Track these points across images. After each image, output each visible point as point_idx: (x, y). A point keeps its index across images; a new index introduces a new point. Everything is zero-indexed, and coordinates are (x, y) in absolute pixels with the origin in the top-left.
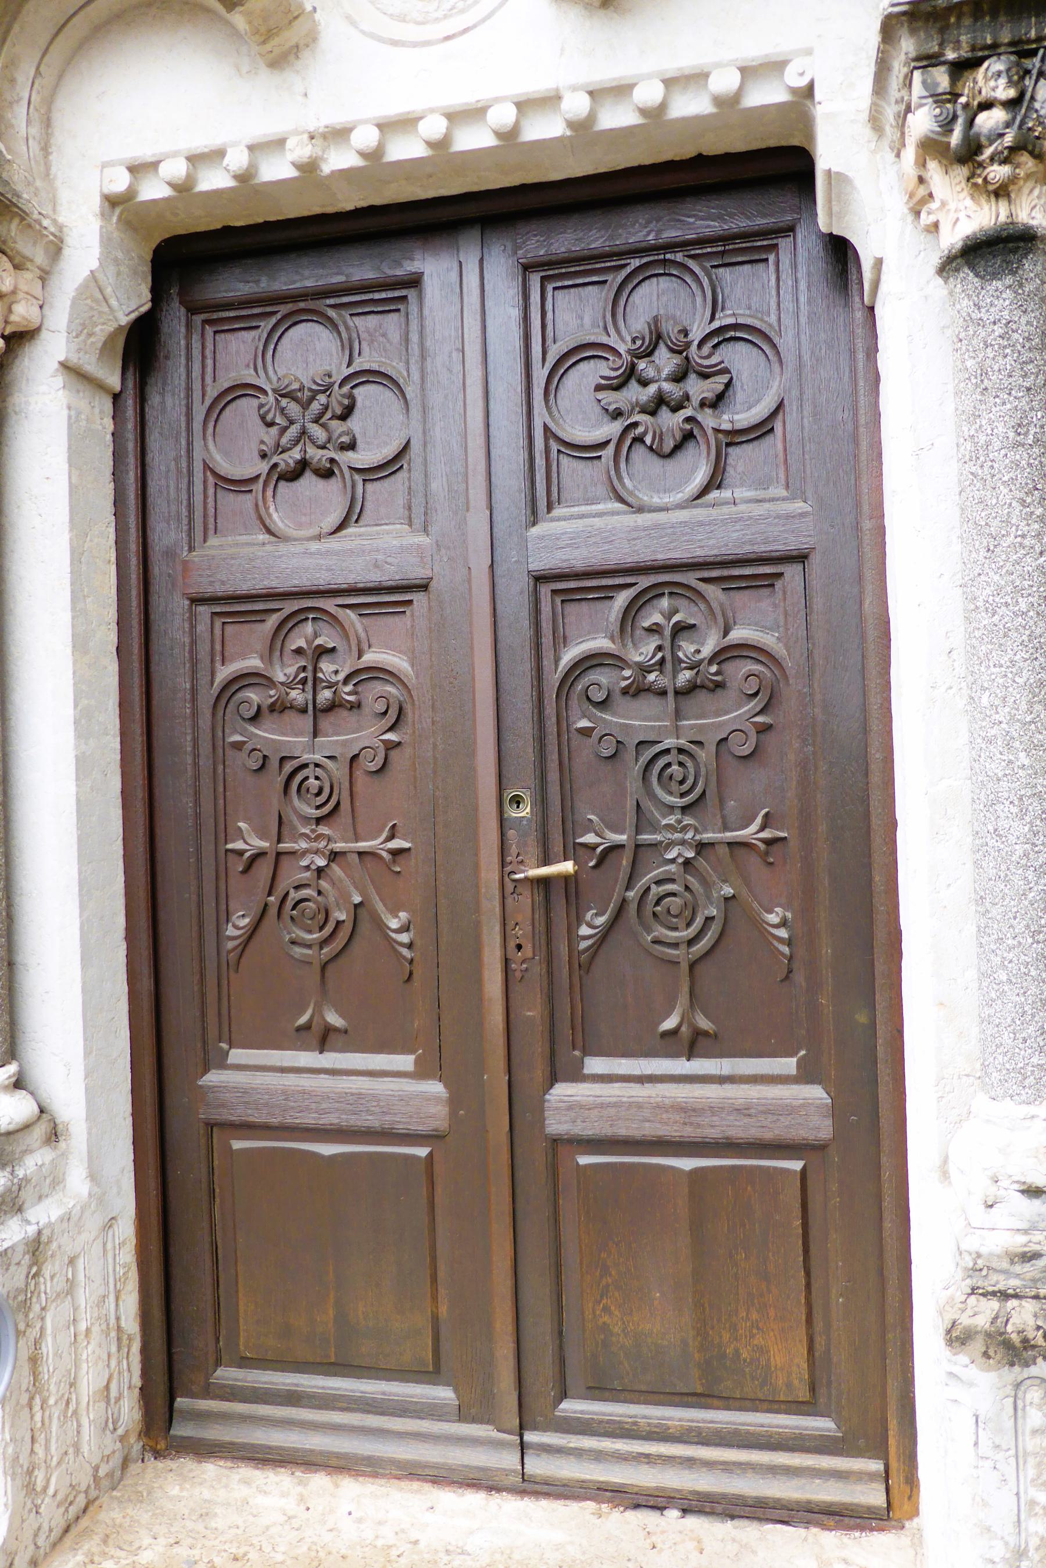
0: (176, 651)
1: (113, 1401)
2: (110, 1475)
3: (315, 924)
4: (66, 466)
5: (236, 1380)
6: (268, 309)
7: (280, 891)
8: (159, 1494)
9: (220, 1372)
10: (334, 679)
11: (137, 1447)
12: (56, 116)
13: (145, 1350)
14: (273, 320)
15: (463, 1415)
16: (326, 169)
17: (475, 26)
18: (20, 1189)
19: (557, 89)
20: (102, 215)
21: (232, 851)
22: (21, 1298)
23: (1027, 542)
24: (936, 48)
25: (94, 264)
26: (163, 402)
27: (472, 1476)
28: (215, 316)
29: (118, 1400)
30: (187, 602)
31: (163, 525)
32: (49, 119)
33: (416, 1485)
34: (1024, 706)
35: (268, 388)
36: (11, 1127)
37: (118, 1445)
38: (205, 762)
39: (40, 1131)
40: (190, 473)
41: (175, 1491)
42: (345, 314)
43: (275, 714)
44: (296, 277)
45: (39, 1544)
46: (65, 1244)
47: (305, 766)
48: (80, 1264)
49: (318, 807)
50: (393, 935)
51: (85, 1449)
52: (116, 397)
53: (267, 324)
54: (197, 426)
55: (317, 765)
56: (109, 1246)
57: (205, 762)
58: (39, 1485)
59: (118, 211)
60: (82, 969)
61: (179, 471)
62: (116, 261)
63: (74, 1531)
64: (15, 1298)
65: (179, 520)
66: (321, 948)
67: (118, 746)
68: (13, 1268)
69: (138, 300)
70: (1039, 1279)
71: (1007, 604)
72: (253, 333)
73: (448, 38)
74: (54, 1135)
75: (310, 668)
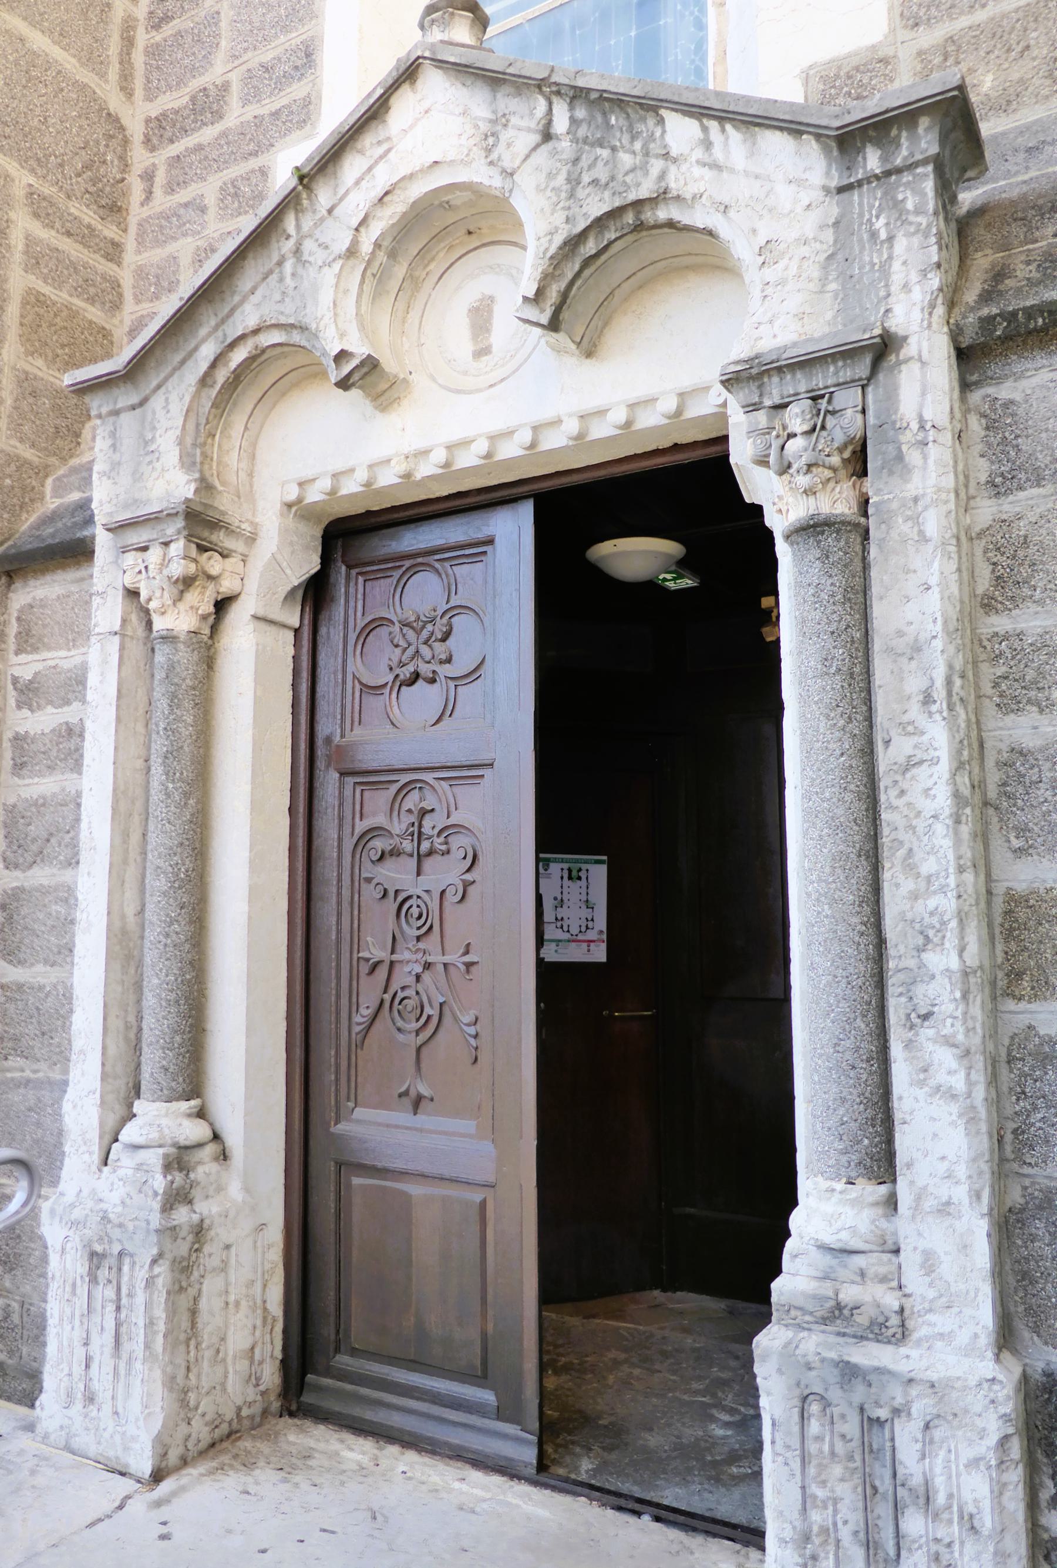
0: (329, 810)
1: (256, 1362)
2: (252, 1417)
3: (413, 1017)
4: (253, 684)
5: (348, 1365)
6: (397, 564)
7: (391, 992)
8: (282, 1438)
9: (338, 1357)
10: (431, 833)
11: (276, 1405)
12: (258, 452)
13: (285, 1331)
14: (401, 571)
15: (500, 1414)
16: (418, 476)
17: (508, 377)
18: (191, 1188)
19: (559, 416)
20: (282, 515)
21: (363, 958)
22: (185, 1264)
23: (830, 746)
24: (757, 399)
25: (274, 549)
26: (328, 633)
27: (501, 1464)
28: (365, 570)
29: (261, 1363)
30: (338, 775)
31: (325, 719)
32: (254, 455)
33: (459, 1464)
34: (827, 870)
35: (394, 619)
36: (188, 1143)
37: (259, 1398)
38: (346, 893)
39: (211, 1149)
40: (344, 682)
41: (292, 1438)
42: (447, 564)
43: (394, 858)
44: (415, 542)
45: (189, 1447)
46: (220, 1234)
47: (409, 897)
48: (233, 1250)
49: (419, 928)
50: (465, 1028)
51: (230, 1389)
52: (297, 631)
53: (397, 574)
54: (350, 649)
55: (418, 897)
56: (259, 1244)
57: (346, 893)
58: (192, 1404)
59: (294, 509)
60: (247, 1037)
61: (336, 682)
62: (291, 544)
63: (218, 1447)
64: (180, 1262)
65: (335, 717)
66: (417, 1035)
67: (287, 879)
68: (179, 1241)
69: (312, 564)
70: (827, 1318)
71: (817, 793)
72: (389, 580)
73: (491, 386)
74: (224, 1156)
75: (416, 824)
